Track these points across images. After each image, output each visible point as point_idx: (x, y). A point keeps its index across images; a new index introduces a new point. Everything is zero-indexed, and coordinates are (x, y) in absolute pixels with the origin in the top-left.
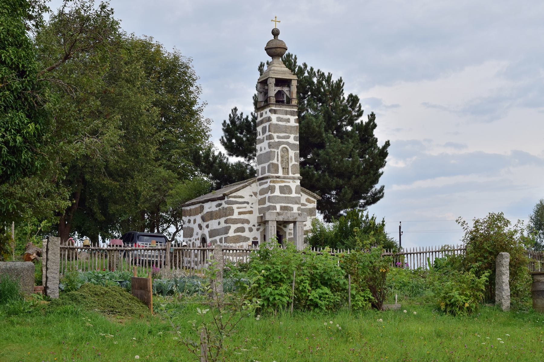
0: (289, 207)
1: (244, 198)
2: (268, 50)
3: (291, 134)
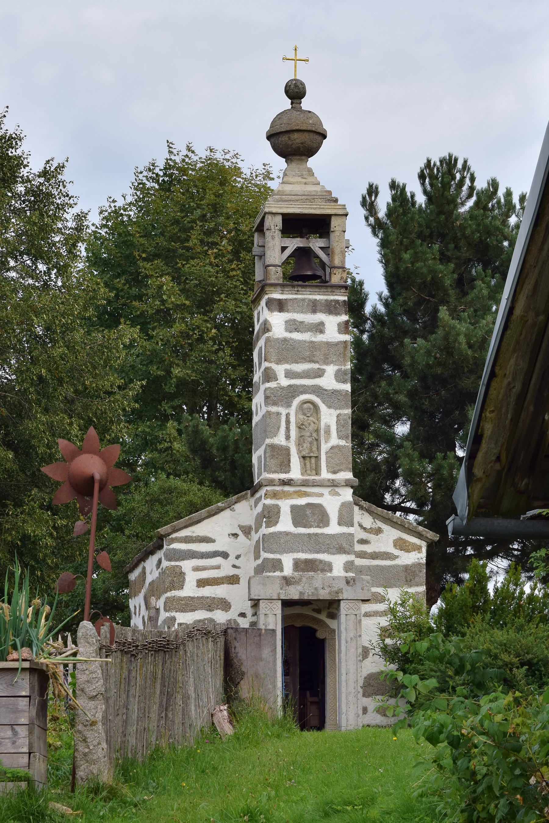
0: (321, 561)
1: (213, 541)
2: (284, 139)
3: (327, 364)
